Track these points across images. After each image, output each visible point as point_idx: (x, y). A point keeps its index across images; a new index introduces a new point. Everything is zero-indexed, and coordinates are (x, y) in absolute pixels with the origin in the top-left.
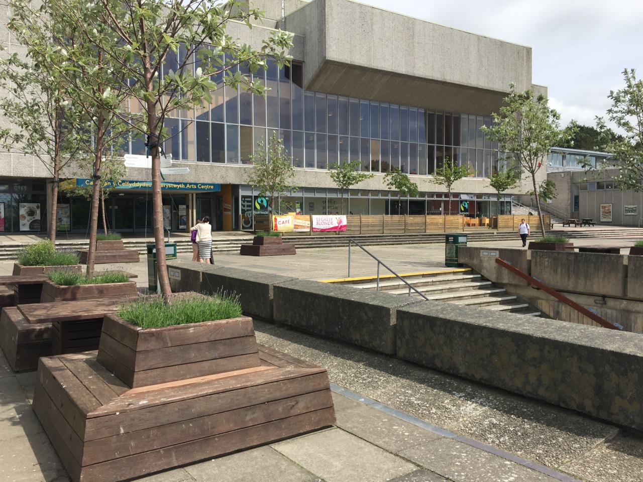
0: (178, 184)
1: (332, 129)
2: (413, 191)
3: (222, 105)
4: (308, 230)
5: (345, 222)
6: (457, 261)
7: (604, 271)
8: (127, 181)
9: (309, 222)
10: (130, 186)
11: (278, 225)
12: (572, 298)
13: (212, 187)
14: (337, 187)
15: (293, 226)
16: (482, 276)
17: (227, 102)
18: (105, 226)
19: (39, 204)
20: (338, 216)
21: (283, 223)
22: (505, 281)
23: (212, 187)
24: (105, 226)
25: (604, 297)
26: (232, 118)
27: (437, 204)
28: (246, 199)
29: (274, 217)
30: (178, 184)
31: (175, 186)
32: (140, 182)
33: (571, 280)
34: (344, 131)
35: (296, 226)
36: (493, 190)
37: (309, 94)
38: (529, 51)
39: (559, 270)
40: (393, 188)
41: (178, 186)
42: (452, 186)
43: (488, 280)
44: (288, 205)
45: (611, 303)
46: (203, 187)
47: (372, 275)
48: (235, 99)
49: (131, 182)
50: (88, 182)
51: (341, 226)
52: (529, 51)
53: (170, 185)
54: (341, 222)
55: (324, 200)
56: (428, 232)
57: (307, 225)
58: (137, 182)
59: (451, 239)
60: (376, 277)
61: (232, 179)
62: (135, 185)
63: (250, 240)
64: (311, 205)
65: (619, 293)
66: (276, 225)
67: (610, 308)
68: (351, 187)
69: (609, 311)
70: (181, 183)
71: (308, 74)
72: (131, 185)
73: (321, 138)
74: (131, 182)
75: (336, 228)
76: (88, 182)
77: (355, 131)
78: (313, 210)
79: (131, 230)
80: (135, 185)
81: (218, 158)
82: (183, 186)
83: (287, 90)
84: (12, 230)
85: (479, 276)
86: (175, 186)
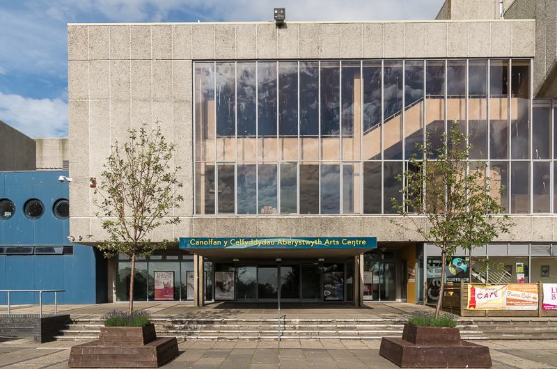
0: (313, 239)
4: (535, 307)
8: (242, 239)
9: (537, 295)
10: (245, 245)
11: (477, 299)
13: (364, 242)
15: (505, 302)
17: (407, 139)
18: (132, 281)
19: (211, 263)
21: (486, 296)
23: (364, 242)
24: (132, 281)
27: (156, 253)
28: (434, 262)
30: (313, 239)
31: (308, 242)
32: (258, 239)
35: (510, 301)
41: (313, 243)
44: (504, 268)
46: (349, 243)
48: (421, 130)
49: (249, 239)
50: (193, 242)
53: (300, 241)
55: (19, 252)
57: (531, 300)
58: (254, 239)
61: (412, 236)
64: (544, 269)
70: (317, 239)
71: (534, 83)
72: (246, 243)
76: (345, 242)
78: (548, 276)
80: (251, 243)
81: (227, 208)
82: (320, 243)
86: (308, 242)
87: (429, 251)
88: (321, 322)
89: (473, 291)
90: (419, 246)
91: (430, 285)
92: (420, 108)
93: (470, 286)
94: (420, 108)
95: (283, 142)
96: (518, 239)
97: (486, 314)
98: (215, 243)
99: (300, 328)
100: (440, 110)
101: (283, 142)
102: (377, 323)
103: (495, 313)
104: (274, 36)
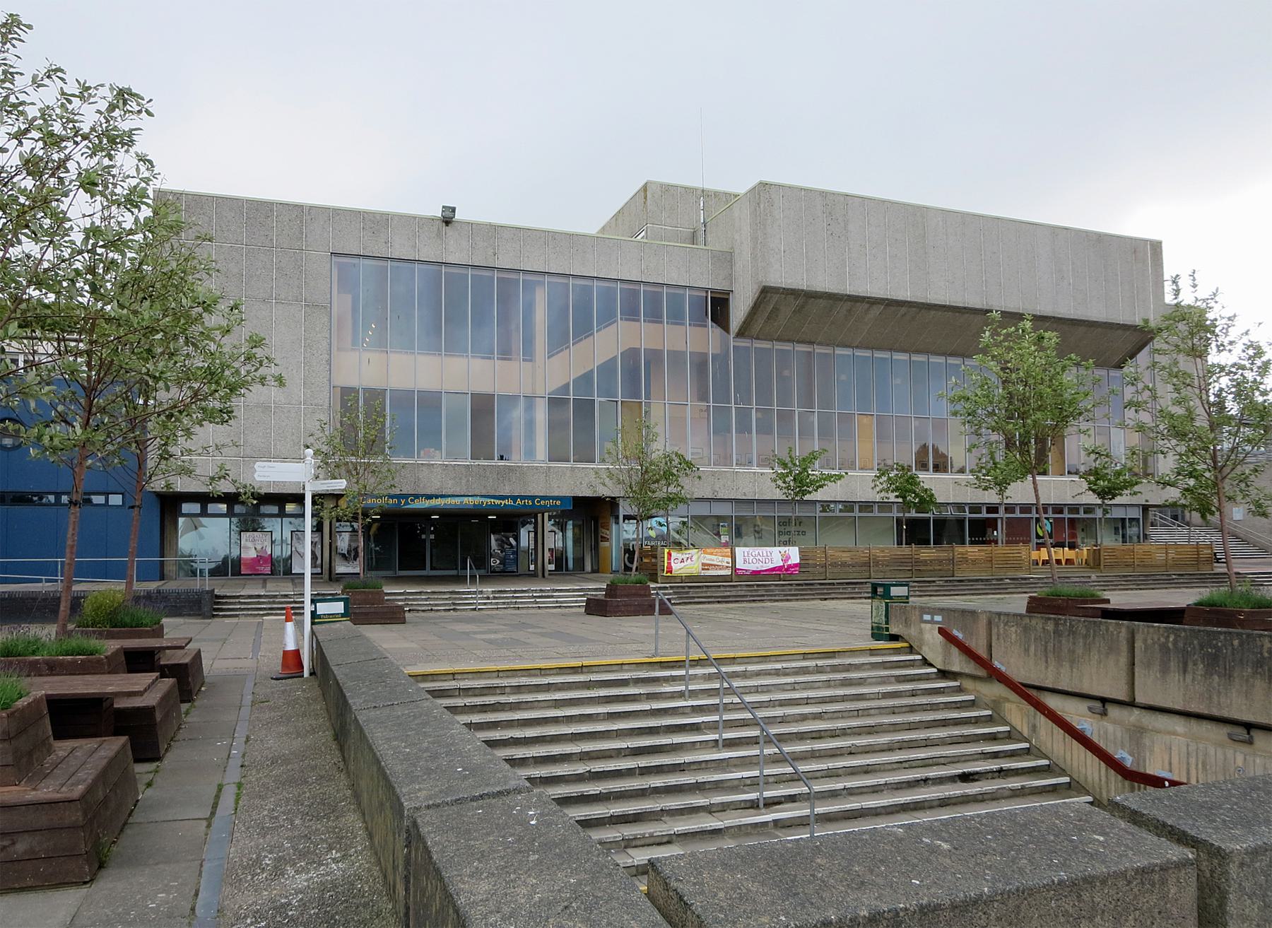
1: (785, 399)
2: (926, 501)
3: (592, 371)
5: (795, 558)
6: (887, 629)
7: (1099, 651)
12: (1053, 702)
13: (558, 503)
14: (784, 497)
16: (924, 659)
20: (783, 549)
21: (682, 561)
22: (956, 668)
23: (558, 503)
25: (1104, 701)
26: (608, 391)
29: (666, 551)
31: (498, 502)
33: (1051, 668)
34: (807, 401)
35: (706, 566)
36: (1092, 499)
37: (743, 343)
38: (1156, 247)
39: (1032, 648)
40: (892, 497)
42: (1007, 493)
43: (931, 665)
45: (1114, 711)
47: (677, 653)
49: (429, 497)
51: (790, 566)
52: (1156, 247)
54: (788, 558)
56: (959, 575)
58: (437, 497)
59: (880, 590)
60: (683, 658)
62: (449, 501)
63: (600, 589)
65: (1121, 695)
66: (669, 563)
67: (1114, 722)
68: (805, 498)
69: (1110, 727)
71: (738, 311)
73: (744, 416)
74: (429, 497)
75: (780, 568)
77: (826, 403)
79: (453, 572)
82: (510, 502)
83: (709, 339)
84: (968, 539)
85: (919, 657)
86: (498, 502)
87: (625, 508)
88: (515, 592)
89: (670, 554)
90: (612, 503)
91: (627, 551)
92: (853, 652)
93: (666, 551)
94: (853, 652)
95: (1037, 496)
96: (720, 496)
97: (682, 579)
98: (391, 501)
99: (495, 598)
100: (805, 656)
101: (1037, 496)
102: (574, 590)
103: (691, 578)
104: (439, 234)
